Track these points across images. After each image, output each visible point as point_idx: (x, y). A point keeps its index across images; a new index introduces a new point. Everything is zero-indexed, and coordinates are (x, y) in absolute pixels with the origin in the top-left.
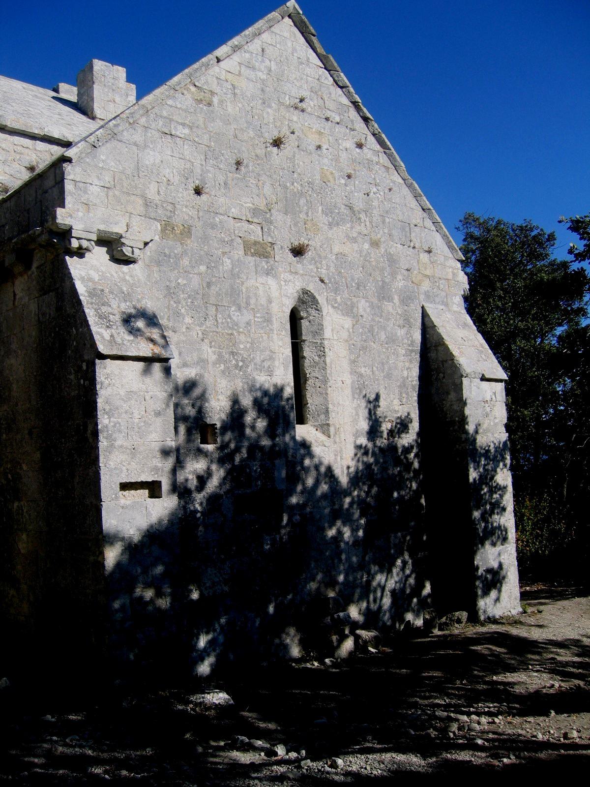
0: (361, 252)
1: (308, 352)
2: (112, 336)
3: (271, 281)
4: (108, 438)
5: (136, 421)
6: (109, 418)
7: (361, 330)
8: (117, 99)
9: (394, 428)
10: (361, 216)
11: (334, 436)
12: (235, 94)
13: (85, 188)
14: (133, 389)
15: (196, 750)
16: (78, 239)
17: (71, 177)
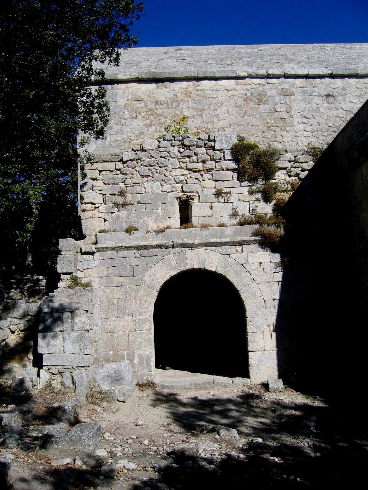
9: (38, 448)
15: (12, 267)
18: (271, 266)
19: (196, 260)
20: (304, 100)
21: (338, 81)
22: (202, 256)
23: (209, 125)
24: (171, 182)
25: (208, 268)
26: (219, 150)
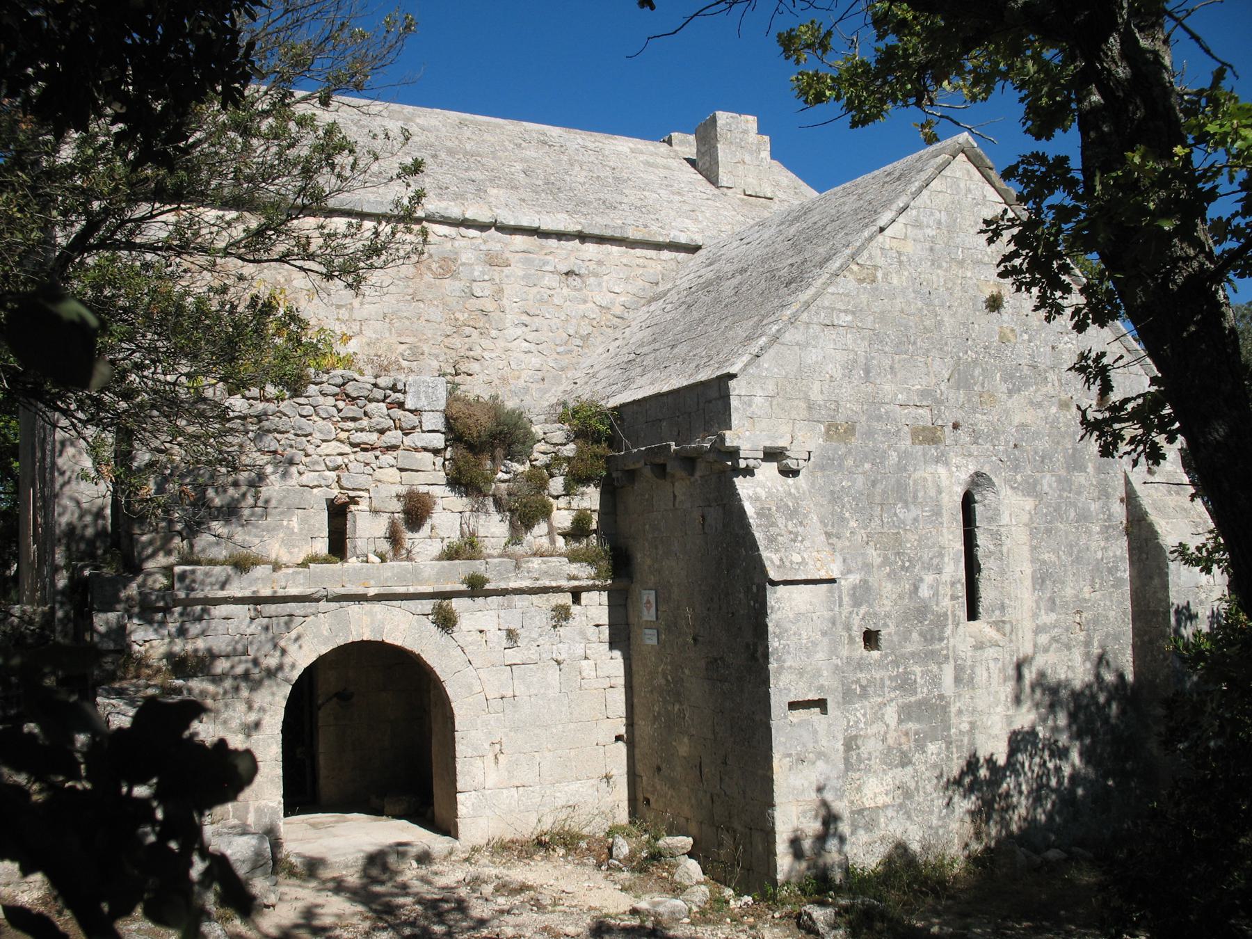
0: (1046, 418)
1: (982, 539)
2: (781, 560)
3: (941, 470)
4: (779, 660)
5: (804, 641)
6: (779, 641)
7: (1045, 511)
8: (747, 158)
10: (1047, 374)
11: (1011, 634)
12: (900, 262)
13: (750, 401)
14: (802, 611)
16: (745, 459)
17: (736, 392)
18: (500, 637)
19: (367, 626)
20: (526, 277)
21: (590, 248)
22: (379, 617)
23: (342, 311)
24: (317, 468)
25: (389, 640)
26: (411, 411)
